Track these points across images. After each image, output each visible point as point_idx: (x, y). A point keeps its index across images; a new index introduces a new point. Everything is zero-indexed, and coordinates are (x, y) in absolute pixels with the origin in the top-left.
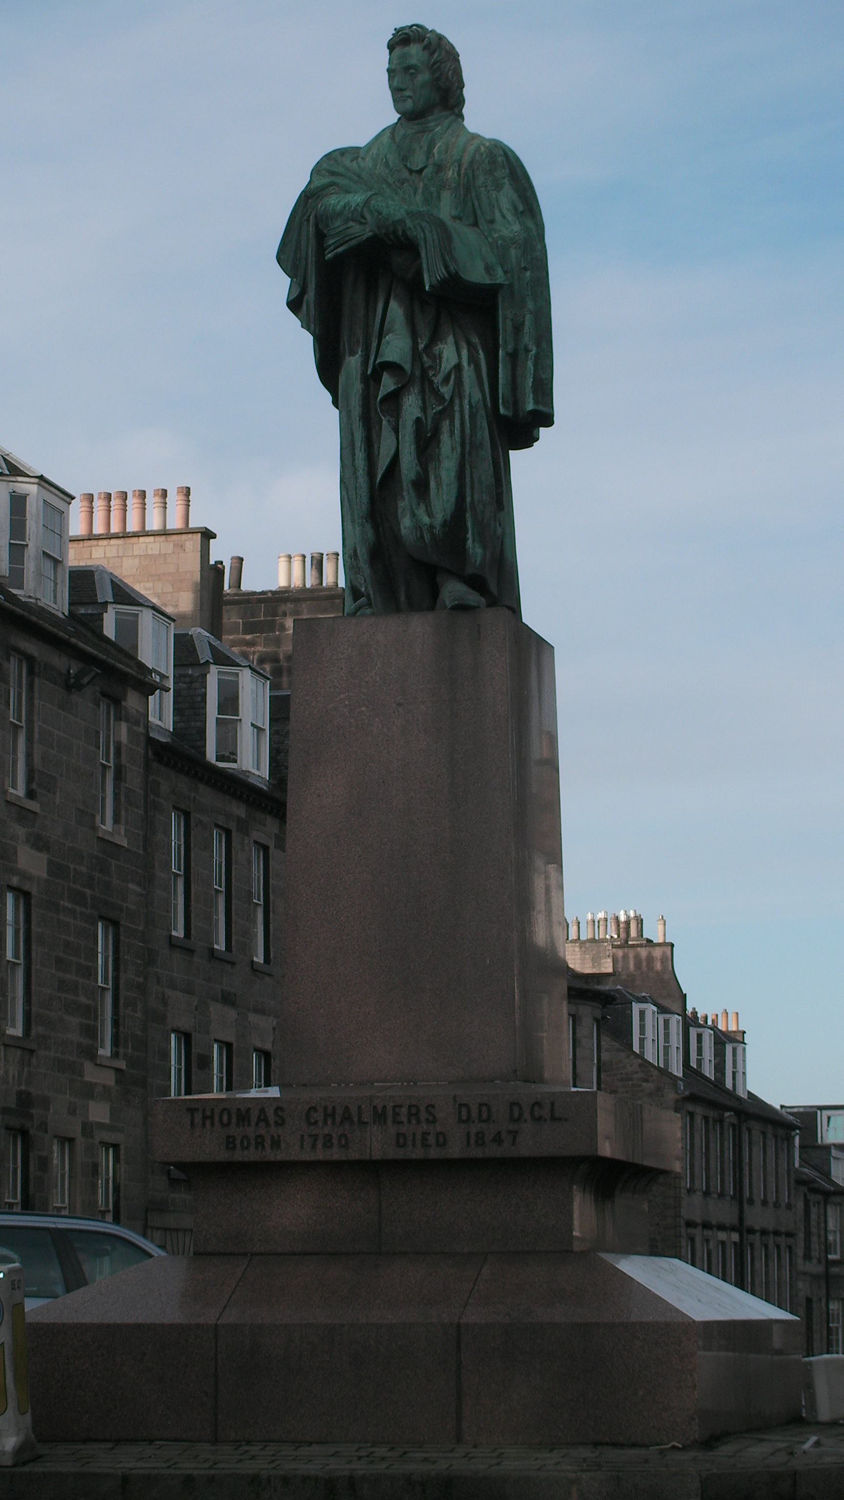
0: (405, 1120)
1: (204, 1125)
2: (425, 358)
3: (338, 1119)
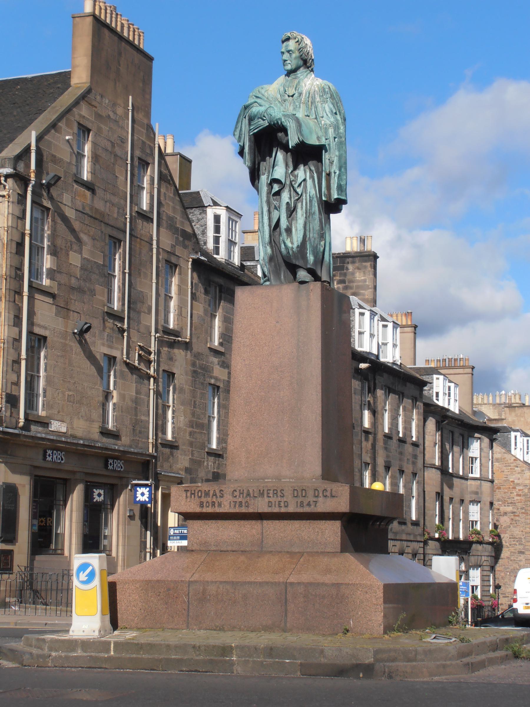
0: (272, 496)
1: (191, 497)
2: (291, 177)
3: (245, 495)
